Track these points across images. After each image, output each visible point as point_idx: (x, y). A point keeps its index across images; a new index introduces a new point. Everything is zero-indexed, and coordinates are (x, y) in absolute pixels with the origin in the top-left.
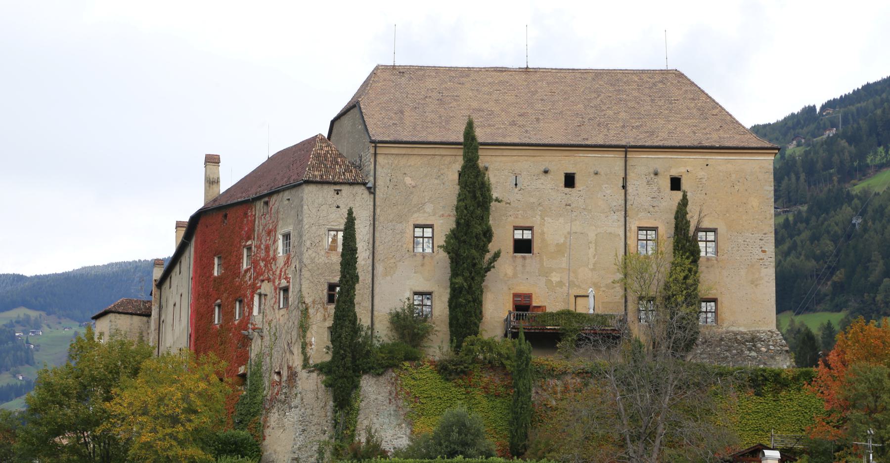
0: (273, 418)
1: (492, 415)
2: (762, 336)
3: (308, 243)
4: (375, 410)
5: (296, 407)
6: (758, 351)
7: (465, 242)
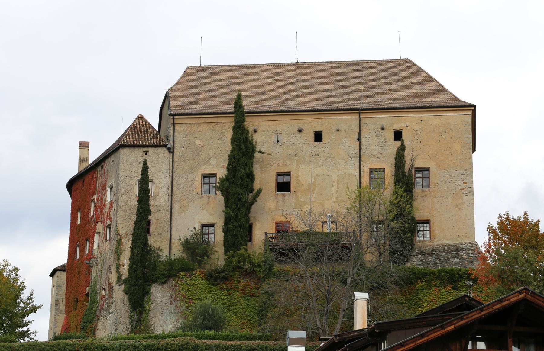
0: (101, 322)
1: (248, 311)
2: (464, 246)
3: (123, 191)
4: (160, 310)
5: (112, 313)
6: (461, 258)
7: (233, 183)
